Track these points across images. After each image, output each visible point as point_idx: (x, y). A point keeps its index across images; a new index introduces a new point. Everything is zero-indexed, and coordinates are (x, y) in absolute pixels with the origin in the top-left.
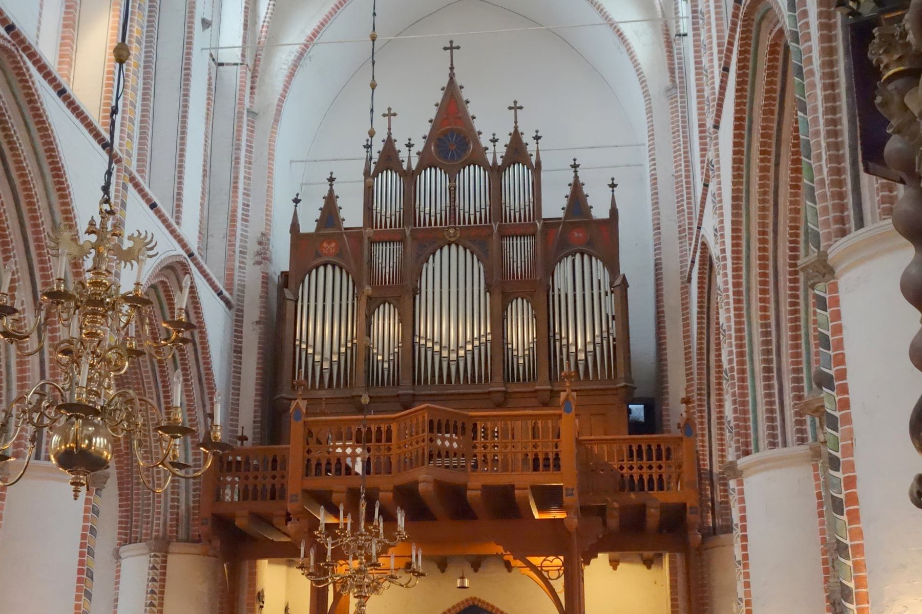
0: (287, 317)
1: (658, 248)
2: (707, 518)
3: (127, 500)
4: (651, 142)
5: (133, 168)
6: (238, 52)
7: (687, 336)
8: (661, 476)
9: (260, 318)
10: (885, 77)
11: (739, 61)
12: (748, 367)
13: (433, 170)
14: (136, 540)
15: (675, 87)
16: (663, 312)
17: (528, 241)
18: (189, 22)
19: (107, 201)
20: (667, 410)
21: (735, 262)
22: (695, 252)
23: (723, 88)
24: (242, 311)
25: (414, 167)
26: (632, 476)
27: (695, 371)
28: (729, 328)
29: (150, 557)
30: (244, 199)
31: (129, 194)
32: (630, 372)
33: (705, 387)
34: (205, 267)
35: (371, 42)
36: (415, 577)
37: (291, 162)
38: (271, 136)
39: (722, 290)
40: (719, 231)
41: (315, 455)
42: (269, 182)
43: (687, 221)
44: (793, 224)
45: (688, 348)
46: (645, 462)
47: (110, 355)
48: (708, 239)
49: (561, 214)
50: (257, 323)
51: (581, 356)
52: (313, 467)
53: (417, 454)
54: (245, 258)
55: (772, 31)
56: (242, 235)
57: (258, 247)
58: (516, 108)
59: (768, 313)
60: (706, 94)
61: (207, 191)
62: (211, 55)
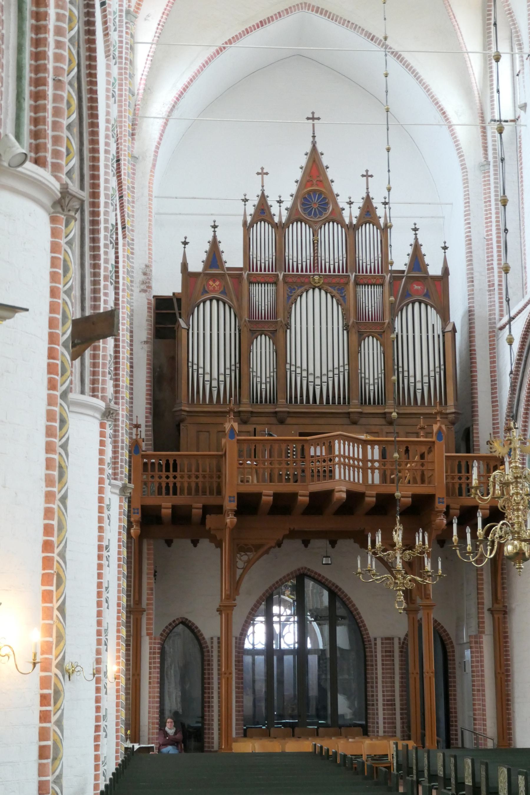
16: (475, 350)
17: (378, 290)
25: (284, 221)
38: (150, 179)
50: (146, 342)
57: (143, 277)
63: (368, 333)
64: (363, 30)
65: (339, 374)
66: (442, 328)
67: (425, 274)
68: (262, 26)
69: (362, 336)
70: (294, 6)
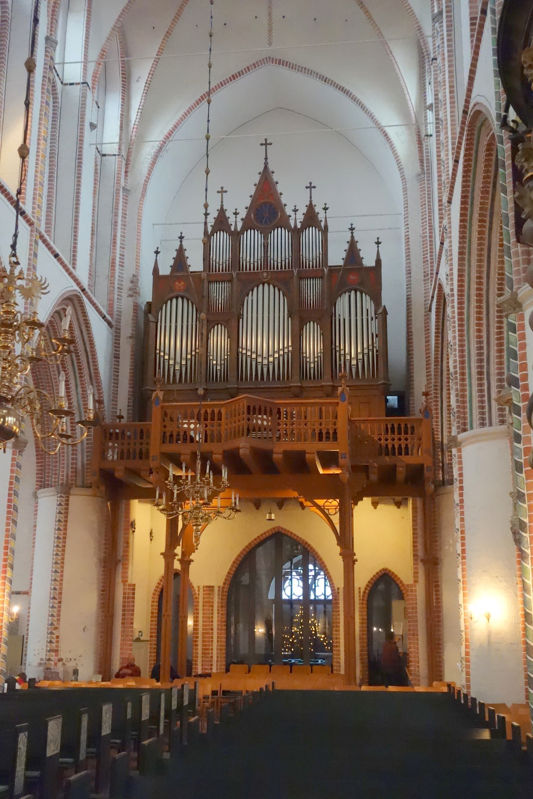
1: (409, 287)
2: (439, 474)
3: (41, 458)
5: (42, 229)
6: (116, 146)
7: (428, 348)
8: (407, 445)
9: (132, 334)
10: (525, 178)
11: (465, 155)
12: (467, 371)
13: (252, 231)
14: (48, 486)
15: (423, 173)
16: (411, 332)
17: (318, 282)
18: (81, 125)
19: (14, 255)
21: (460, 298)
22: (434, 290)
23: (454, 174)
24: (120, 329)
26: (387, 445)
27: (433, 373)
30: (120, 251)
32: (387, 372)
33: (439, 384)
34: (94, 298)
36: (234, 513)
37: (153, 225)
39: (450, 317)
40: (449, 276)
41: (169, 430)
42: (138, 239)
43: (429, 269)
44: (501, 272)
46: (396, 436)
47: (18, 361)
48: (443, 281)
49: (341, 263)
50: (131, 337)
51: (354, 362)
52: (168, 438)
53: (243, 428)
54: (122, 292)
55: (488, 134)
56: (119, 276)
57: (130, 285)
58: (311, 187)
59: (481, 334)
60: (443, 178)
61: (95, 245)
62: (97, 149)
64: (317, 74)
65: (284, 355)
68: (234, 79)
70: (260, 61)
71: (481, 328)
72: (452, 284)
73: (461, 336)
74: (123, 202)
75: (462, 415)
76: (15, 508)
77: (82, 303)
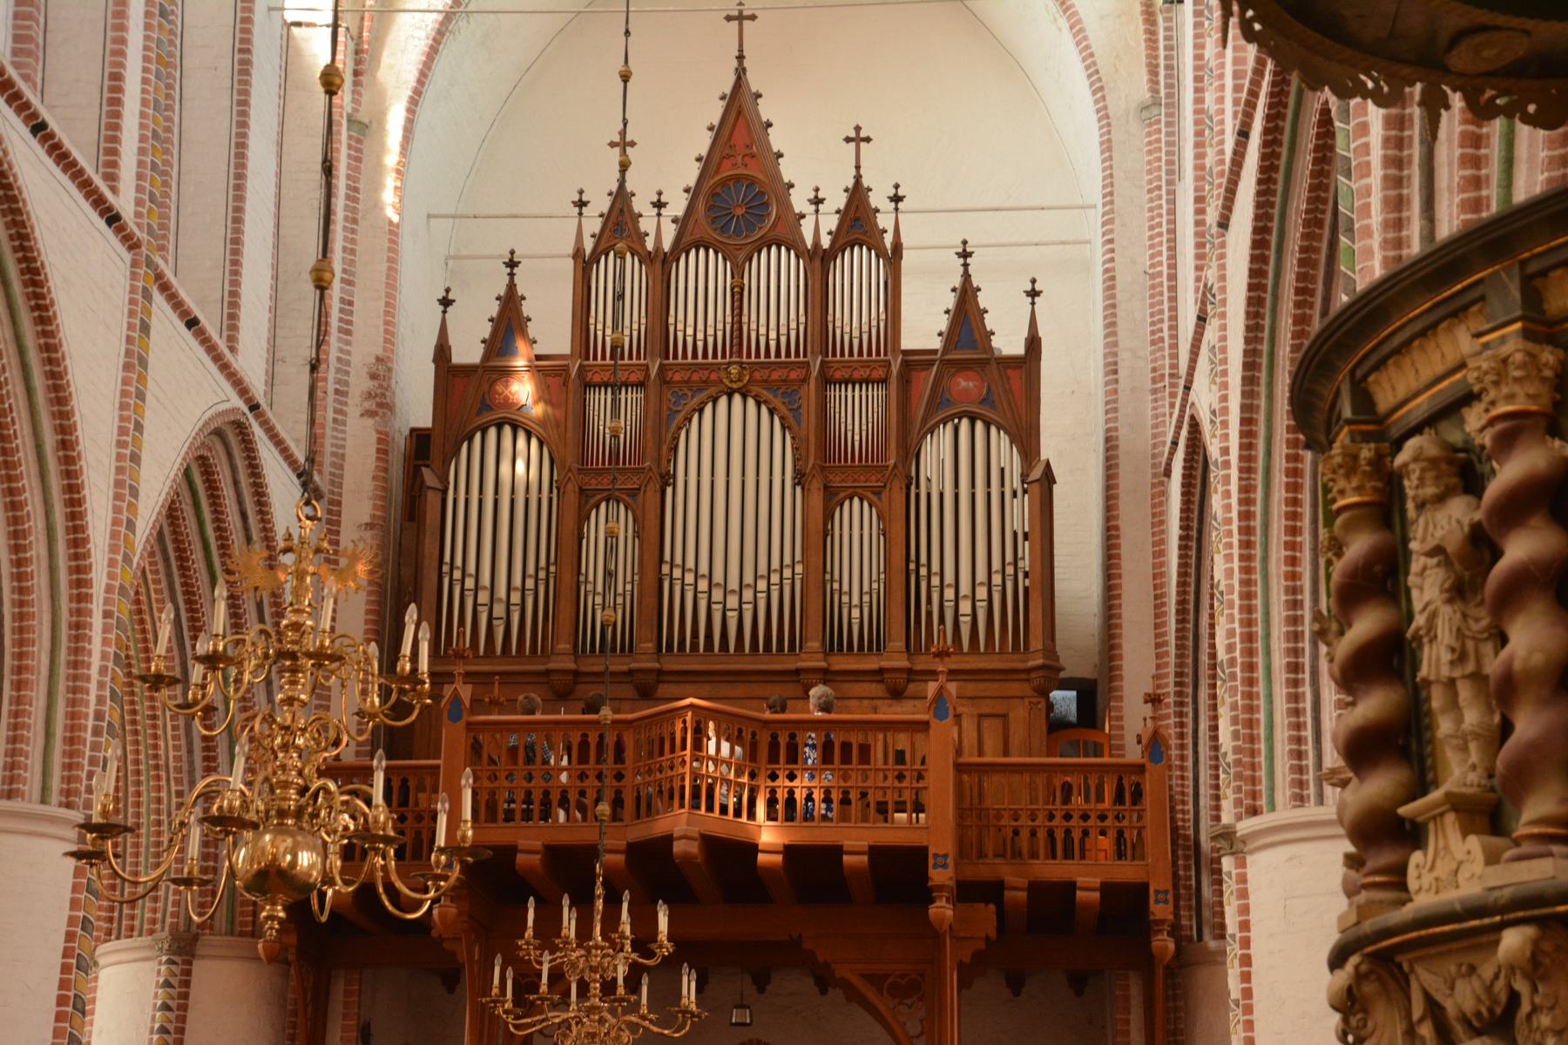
0: (428, 521)
1: (1111, 407)
4: (1107, 208)
7: (1159, 575)
12: (1260, 660)
16: (1117, 528)
17: (875, 393)
20: (1120, 709)
21: (1245, 476)
22: (1179, 427)
24: (339, 503)
28: (1231, 589)
29: (160, 964)
30: (342, 291)
31: (154, 308)
32: (1053, 638)
35: (622, 84)
37: (429, 216)
39: (1219, 519)
42: (390, 260)
43: (1167, 362)
45: (1159, 596)
49: (936, 343)
50: (370, 526)
56: (339, 360)
57: (370, 384)
58: (858, 139)
60: (1209, 161)
63: (850, 491)
66: (1022, 475)
67: (986, 353)
69: (832, 499)
71: (1299, 510)
72: (1227, 435)
73: (1247, 570)
74: (349, 156)
75: (1248, 773)
76: (79, 1006)
77: (250, 442)
